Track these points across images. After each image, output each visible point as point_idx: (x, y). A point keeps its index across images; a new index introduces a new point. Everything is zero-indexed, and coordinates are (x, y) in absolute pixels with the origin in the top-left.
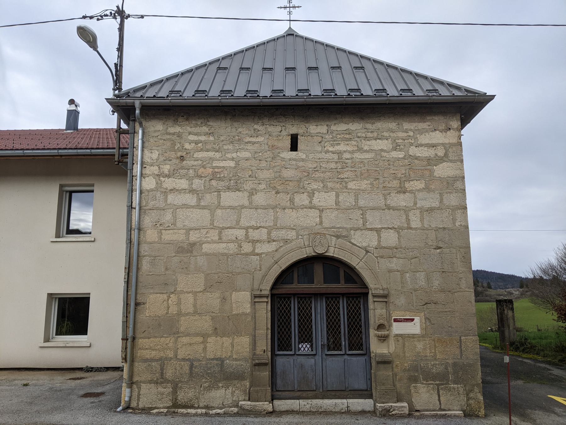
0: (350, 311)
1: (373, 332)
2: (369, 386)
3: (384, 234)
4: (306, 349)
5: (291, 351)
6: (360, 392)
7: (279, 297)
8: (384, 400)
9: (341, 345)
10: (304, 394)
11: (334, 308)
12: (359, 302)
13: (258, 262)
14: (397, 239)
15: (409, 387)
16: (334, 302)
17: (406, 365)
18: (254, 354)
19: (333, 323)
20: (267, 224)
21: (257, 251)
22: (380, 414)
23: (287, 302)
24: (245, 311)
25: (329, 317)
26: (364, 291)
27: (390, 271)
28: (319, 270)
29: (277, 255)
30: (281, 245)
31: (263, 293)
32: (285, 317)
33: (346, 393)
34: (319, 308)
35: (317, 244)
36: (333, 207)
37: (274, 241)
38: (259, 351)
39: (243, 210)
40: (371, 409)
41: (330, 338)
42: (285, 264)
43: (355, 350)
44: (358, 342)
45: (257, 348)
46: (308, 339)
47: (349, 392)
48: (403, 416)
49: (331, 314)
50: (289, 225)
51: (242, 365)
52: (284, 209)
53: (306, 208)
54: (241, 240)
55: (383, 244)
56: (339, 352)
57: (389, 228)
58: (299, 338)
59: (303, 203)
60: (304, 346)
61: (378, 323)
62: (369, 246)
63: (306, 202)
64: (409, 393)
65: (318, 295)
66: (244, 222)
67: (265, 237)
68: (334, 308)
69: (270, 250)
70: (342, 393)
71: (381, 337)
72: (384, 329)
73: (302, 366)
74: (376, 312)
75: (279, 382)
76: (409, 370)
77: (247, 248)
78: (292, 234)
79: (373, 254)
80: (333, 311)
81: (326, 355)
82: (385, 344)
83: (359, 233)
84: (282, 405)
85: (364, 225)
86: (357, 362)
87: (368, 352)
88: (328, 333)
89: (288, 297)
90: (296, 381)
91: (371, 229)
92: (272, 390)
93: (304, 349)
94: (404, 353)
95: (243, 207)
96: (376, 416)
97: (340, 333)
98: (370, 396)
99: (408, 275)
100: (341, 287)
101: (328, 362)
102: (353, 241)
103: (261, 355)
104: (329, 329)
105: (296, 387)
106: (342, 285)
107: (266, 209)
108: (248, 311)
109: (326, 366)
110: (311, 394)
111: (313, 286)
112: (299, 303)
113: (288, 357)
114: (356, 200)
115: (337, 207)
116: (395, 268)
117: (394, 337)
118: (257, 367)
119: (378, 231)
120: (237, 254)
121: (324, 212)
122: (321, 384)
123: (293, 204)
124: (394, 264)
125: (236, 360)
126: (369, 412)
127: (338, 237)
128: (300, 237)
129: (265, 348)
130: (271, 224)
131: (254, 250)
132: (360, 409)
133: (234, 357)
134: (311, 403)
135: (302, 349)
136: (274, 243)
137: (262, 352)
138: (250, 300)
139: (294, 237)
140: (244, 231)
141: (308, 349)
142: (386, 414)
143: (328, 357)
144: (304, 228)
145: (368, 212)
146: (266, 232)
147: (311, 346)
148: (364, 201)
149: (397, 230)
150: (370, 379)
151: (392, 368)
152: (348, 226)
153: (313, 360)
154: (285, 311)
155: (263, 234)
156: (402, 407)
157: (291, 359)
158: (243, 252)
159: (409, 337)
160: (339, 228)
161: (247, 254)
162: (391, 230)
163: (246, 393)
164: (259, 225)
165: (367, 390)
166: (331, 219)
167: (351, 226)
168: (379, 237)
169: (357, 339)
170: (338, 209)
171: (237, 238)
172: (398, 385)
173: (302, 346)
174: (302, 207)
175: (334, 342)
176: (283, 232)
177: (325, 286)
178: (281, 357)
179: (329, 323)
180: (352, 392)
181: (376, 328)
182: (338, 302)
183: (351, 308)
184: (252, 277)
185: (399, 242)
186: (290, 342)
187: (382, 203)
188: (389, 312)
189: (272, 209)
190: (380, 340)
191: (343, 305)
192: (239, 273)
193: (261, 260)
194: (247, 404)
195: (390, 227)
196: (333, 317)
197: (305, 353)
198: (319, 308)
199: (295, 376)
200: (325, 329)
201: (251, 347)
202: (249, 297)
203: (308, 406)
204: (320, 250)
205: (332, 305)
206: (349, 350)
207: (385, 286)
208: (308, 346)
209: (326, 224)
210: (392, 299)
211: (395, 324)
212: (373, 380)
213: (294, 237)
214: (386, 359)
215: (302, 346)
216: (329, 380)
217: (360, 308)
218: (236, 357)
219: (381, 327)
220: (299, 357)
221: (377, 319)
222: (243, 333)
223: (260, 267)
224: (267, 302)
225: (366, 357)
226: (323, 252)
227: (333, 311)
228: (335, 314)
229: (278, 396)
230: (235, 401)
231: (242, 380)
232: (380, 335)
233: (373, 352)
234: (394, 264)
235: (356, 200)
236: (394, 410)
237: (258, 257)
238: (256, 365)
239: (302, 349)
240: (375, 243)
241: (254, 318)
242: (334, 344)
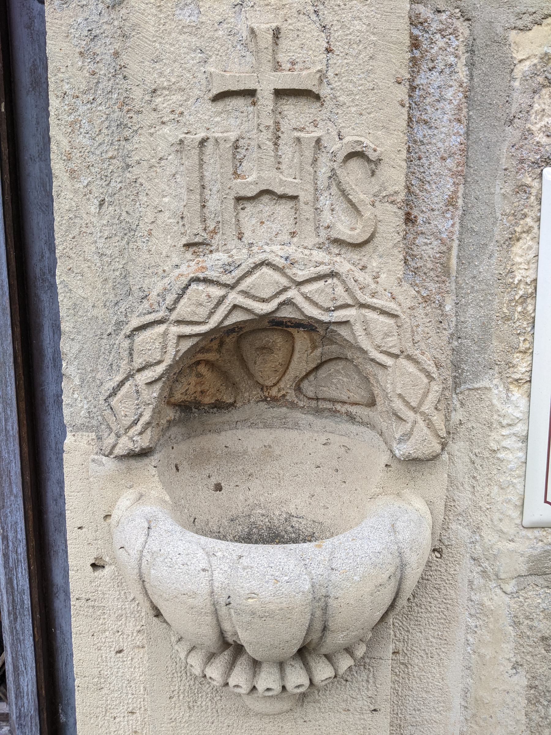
72: (325, 407)
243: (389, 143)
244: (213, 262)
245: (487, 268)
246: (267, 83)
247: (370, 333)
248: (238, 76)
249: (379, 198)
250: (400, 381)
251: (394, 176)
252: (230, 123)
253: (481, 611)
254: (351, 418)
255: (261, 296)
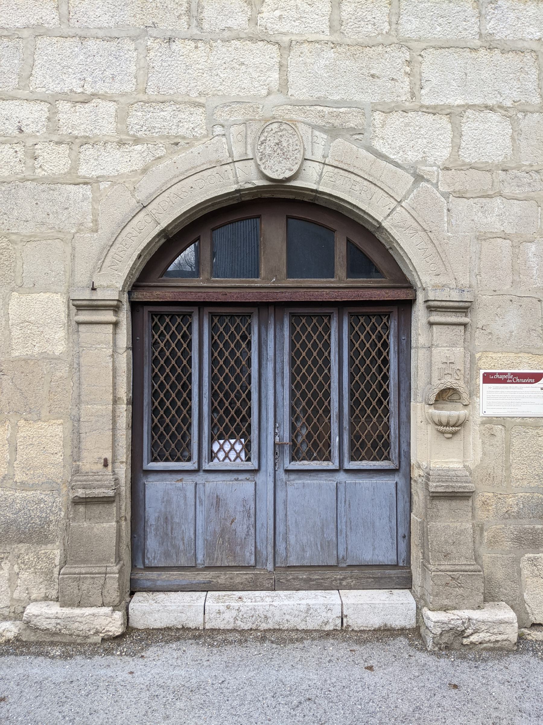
0: (357, 353)
1: (420, 412)
2: (403, 555)
3: (471, 125)
4: (232, 455)
5: (189, 460)
6: (378, 573)
7: (161, 316)
8: (446, 602)
9: (328, 445)
10: (223, 578)
11: (315, 345)
12: (386, 328)
13: (87, 206)
14: (508, 142)
15: (517, 561)
16: (315, 329)
17: (511, 501)
18: (77, 471)
19: (309, 386)
20: (116, 88)
21: (84, 171)
22: (436, 644)
23: (179, 328)
24: (49, 348)
25: (298, 370)
26: (401, 295)
27: (481, 238)
28: (274, 236)
29: (147, 187)
30: (159, 153)
31: (99, 295)
32: (173, 370)
33: (339, 575)
34: (271, 344)
35: (268, 151)
36: (322, 37)
37: (137, 141)
38: (90, 462)
39: (42, 42)
40: (410, 622)
41: (299, 425)
42: (168, 212)
43: (369, 457)
44: (376, 436)
45: (84, 454)
46: (238, 429)
47: (348, 573)
48: (501, 649)
49: (304, 362)
50: (183, 90)
51: (40, 501)
52: (170, 40)
53: (238, 39)
54: (33, 135)
55: (468, 156)
56: (325, 465)
57: (486, 107)
58: (213, 426)
59: (230, 23)
60: (227, 447)
61: (438, 385)
62: (424, 161)
63: (239, 21)
64: (516, 578)
65: (270, 308)
66: (44, 81)
67: (108, 128)
68: (315, 345)
69: (125, 169)
70: (329, 574)
71: (448, 425)
72: (452, 401)
73: (218, 502)
74: (431, 353)
75: (152, 543)
76: (519, 516)
77: (54, 161)
78: (193, 122)
79: (436, 185)
80: (309, 354)
81: (287, 471)
82: (456, 442)
83: (397, 120)
84: (153, 609)
85: (413, 95)
86: (372, 492)
87: (403, 464)
88: (293, 411)
89: (182, 311)
90: (200, 543)
91: (433, 111)
92: (133, 567)
93: (227, 456)
94: (508, 469)
95: (39, 31)
96: (423, 648)
97: (327, 411)
98: (406, 583)
99: (533, 248)
100: (339, 284)
101: (290, 489)
102: (378, 145)
103: (96, 473)
104: (298, 403)
105: (200, 557)
106: (340, 281)
107: (112, 39)
108: (60, 348)
109: (285, 502)
110: (241, 577)
111: (258, 282)
112: (213, 329)
113: (179, 477)
114: (395, 20)
115: (336, 38)
116: (498, 227)
117: (483, 423)
118: (81, 509)
119: (454, 114)
120: (24, 180)
121: (296, 50)
122: (270, 549)
123: (199, 25)
124: (496, 216)
125: (23, 486)
126: (402, 631)
127: (333, 132)
128: (218, 130)
129: (108, 455)
130: (129, 87)
131: (75, 167)
132: (376, 622)
133: (17, 478)
134: (235, 604)
135: (221, 455)
136: (139, 147)
137: (101, 466)
138: (63, 317)
139: (200, 132)
140: (45, 107)
141: (238, 456)
142: (454, 644)
143: (293, 477)
144: (230, 104)
145: (430, 56)
146: (112, 111)
147: (247, 447)
148: (416, 22)
149: (512, 113)
150: (408, 537)
151: (473, 509)
152: (366, 99)
153: (249, 487)
154: (173, 353)
155: (101, 119)
156: (501, 622)
157: (188, 481)
158: (40, 173)
159: (524, 425)
160: (338, 104)
161: (53, 181)
162: (491, 114)
163: (51, 580)
164: (89, 90)
165: (396, 566)
166: (315, 75)
167: (376, 99)
168: (458, 133)
169: (375, 428)
170: (335, 45)
171: (21, 131)
172: (486, 556)
173: (221, 448)
174: (226, 34)
175: (309, 436)
176: (168, 112)
177: (291, 282)
178: (159, 476)
179: (298, 386)
180: (356, 572)
181: (433, 399)
182: (327, 329)
183: (363, 345)
184: (69, 250)
185: (516, 149)
186: (186, 436)
187: (469, 30)
188: (472, 356)
189: (133, 39)
190: (443, 433)
191: (339, 337)
192: (29, 239)
193: (95, 200)
194: (46, 613)
195: (490, 103)
196: (309, 370)
197: (228, 465)
198: (271, 344)
199: (200, 531)
200: (287, 402)
201: (68, 451)
202: (63, 308)
203: (228, 616)
204: (278, 171)
205: (309, 337)
206: (352, 459)
207: (464, 281)
208: (238, 447)
209: (300, 90)
210: (479, 318)
211: (487, 389)
212: (415, 539)
213: (200, 132)
214: (458, 486)
215: (221, 448)
216: (292, 539)
217: (386, 345)
218: (25, 478)
219: (446, 395)
220: (211, 477)
221: (435, 375)
222: (44, 412)
223: (95, 221)
224: (116, 324)
225: (397, 478)
226: (288, 174)
227: (309, 354)
228: (315, 362)
229: (148, 584)
230: (19, 600)
231: (39, 543)
232: (444, 420)
233: (419, 467)
234: (496, 216)
235: (395, 20)
236: (476, 632)
237: (87, 190)
238: (77, 502)
239: (221, 455)
240: (442, 153)
241: (76, 368)
242: (309, 442)
243: (462, 368)
244: (442, 381)
245: (473, 382)
246: (448, 362)
247: (461, 390)
248: (445, 361)
249: (461, 374)
250: (464, 395)
251: (462, 372)
252: (444, 366)
253: (474, 430)
254: (456, 402)
255: (449, 385)
